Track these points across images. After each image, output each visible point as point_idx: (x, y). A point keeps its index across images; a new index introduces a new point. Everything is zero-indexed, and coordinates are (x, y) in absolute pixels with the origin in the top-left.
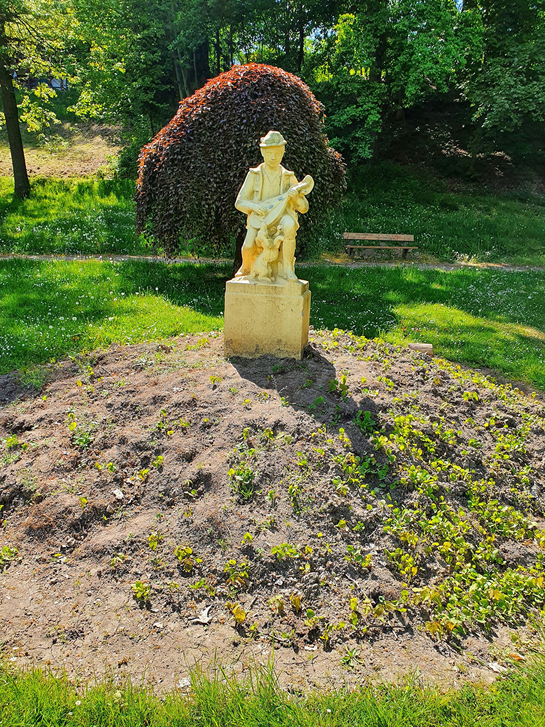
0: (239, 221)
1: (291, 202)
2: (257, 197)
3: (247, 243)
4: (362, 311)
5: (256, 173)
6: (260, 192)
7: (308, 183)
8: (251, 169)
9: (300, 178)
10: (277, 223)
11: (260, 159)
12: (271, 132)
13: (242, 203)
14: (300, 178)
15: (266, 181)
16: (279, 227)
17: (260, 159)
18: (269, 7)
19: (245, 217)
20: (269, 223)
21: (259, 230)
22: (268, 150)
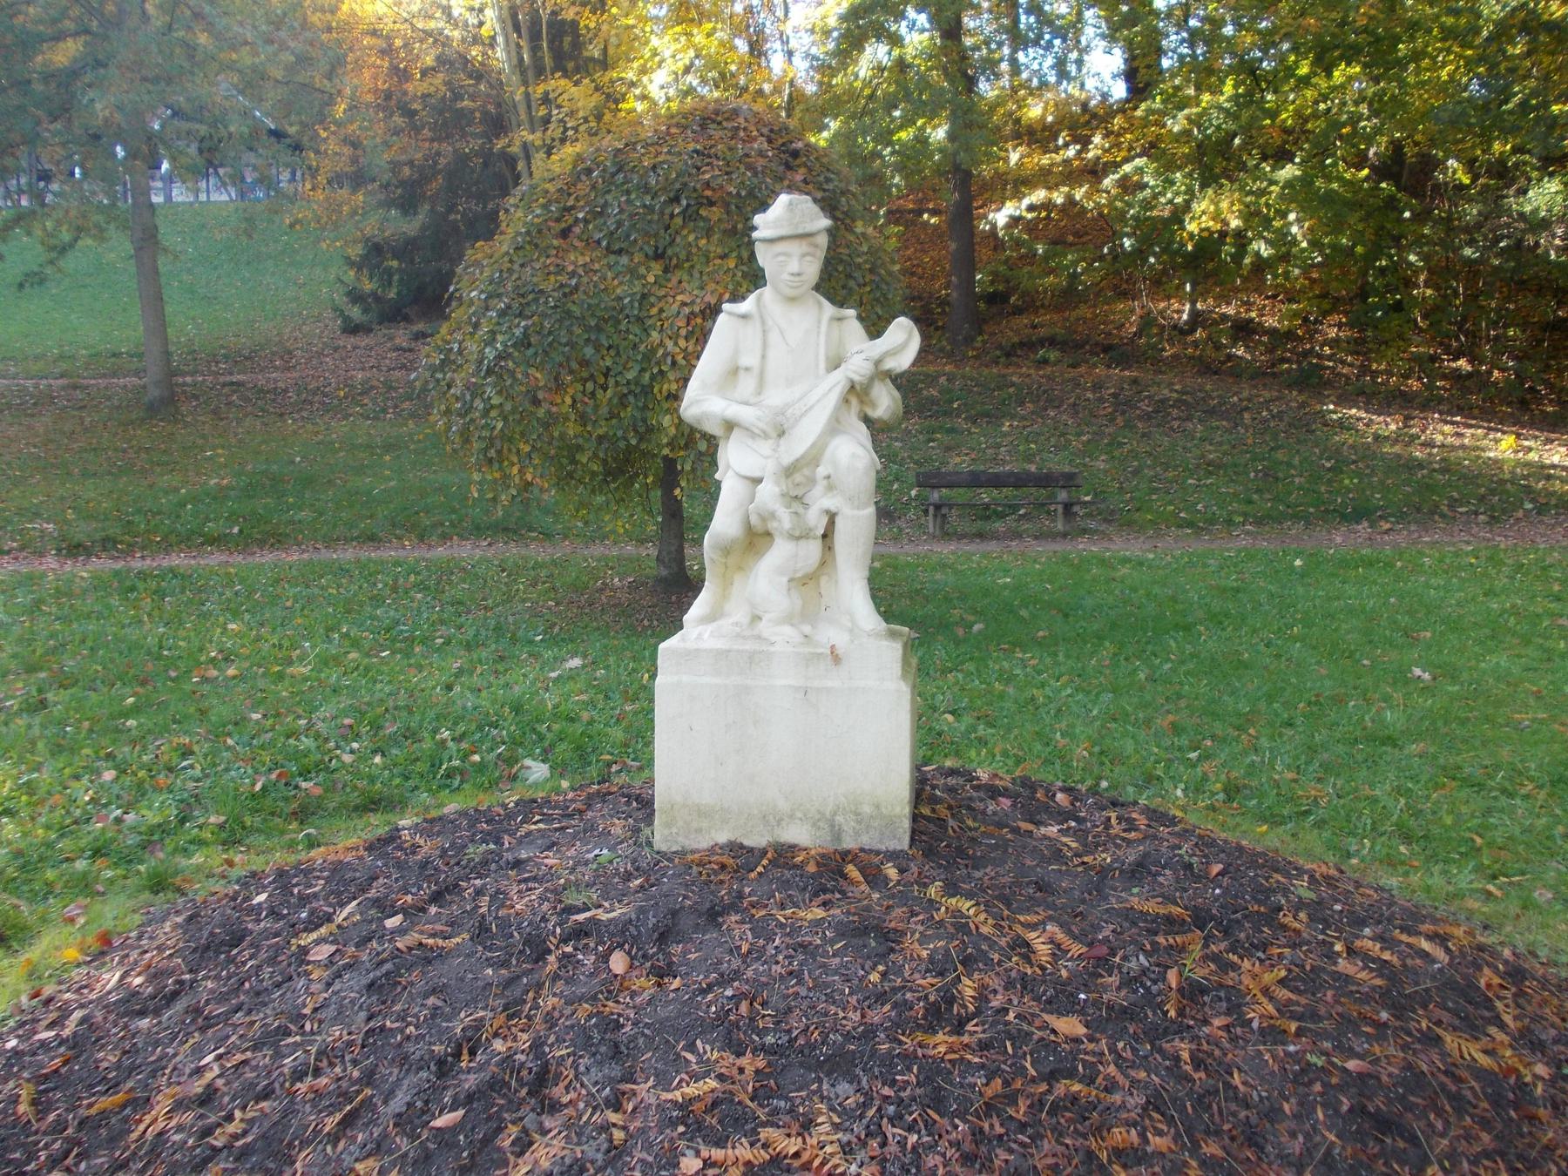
0: (697, 451)
1: (857, 392)
2: (747, 385)
3: (724, 522)
4: (1160, 52)
5: (744, 317)
6: (756, 371)
7: (902, 341)
8: (726, 306)
9: (875, 328)
10: (812, 458)
11: (756, 279)
12: (783, 199)
13: (703, 399)
14: (875, 328)
15: (774, 337)
16: (822, 471)
17: (756, 279)
18: (174, 1168)
19: (712, 442)
20: (787, 460)
21: (759, 481)
22: (780, 247)
